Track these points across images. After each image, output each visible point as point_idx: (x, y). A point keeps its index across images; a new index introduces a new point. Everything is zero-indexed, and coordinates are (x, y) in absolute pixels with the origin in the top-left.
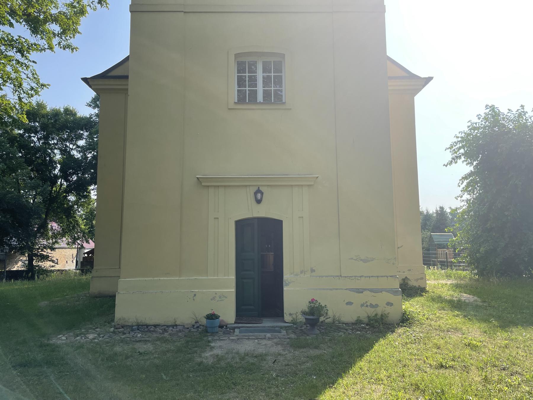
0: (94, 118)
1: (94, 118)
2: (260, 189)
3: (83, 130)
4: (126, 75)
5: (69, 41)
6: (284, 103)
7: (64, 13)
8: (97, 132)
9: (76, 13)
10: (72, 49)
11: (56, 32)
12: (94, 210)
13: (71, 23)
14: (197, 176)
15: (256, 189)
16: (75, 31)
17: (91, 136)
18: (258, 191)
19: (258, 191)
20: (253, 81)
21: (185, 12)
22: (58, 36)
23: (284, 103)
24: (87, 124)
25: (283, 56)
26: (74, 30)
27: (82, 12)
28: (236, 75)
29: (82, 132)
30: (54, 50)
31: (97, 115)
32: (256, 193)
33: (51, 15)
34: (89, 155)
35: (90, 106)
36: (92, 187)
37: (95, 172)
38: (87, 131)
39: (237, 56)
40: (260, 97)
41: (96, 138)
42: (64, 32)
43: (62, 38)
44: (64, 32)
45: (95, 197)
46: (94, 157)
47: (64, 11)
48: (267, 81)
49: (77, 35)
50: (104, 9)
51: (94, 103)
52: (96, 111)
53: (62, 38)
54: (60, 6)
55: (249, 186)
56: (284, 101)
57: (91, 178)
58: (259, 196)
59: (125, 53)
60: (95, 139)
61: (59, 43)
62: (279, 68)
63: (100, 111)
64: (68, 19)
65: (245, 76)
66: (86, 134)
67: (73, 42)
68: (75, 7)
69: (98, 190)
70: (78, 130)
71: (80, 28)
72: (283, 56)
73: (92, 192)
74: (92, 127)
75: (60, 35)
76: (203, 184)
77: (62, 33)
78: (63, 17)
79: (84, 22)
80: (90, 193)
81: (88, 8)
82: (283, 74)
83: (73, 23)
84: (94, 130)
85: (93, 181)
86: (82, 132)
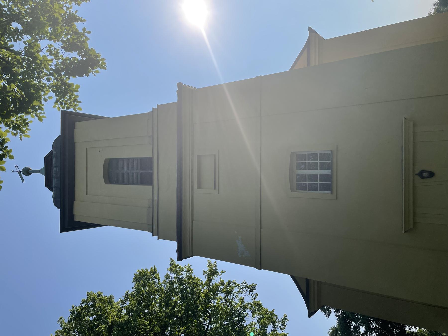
0: (339, 314)
1: (339, 314)
2: (417, 172)
3: (351, 326)
4: (305, 281)
5: (279, 321)
6: (331, 151)
7: (259, 319)
8: (353, 315)
9: (260, 311)
10: (286, 319)
11: (273, 329)
12: (431, 332)
13: (266, 316)
14: (403, 232)
15: (417, 177)
16: (272, 313)
17: (357, 320)
18: (421, 174)
19: (421, 174)
20: (314, 177)
21: (261, 228)
22: (276, 328)
23: (331, 151)
24: (344, 321)
25: (292, 153)
26: (271, 314)
27: (258, 305)
28: (307, 191)
29: (352, 327)
30: (286, 333)
31: (336, 311)
32: (423, 177)
33: (261, 330)
34: (374, 325)
35: (328, 315)
36: (407, 329)
37: (391, 323)
38: (352, 322)
39: (292, 190)
40: (327, 172)
41: (358, 316)
42: (273, 323)
43: (277, 326)
44: (273, 323)
45: (418, 328)
46: (376, 321)
47: (257, 319)
48: (311, 167)
49: (275, 313)
50: (257, 288)
51: (327, 311)
52: (333, 310)
53: (277, 326)
54: (254, 321)
55: (414, 183)
56: (330, 152)
57: (398, 329)
58: (425, 174)
59: (287, 278)
60: (359, 317)
61: (281, 329)
62: (302, 157)
63: (333, 307)
64: (263, 317)
65: (308, 184)
66: (353, 323)
67: (280, 317)
68: (255, 310)
69: (410, 324)
70: (350, 330)
71: (270, 310)
72: (292, 153)
73: (412, 330)
74: (347, 317)
75: (275, 327)
76: (412, 227)
77: (274, 325)
78: (262, 320)
79: (267, 305)
80: (413, 332)
81: (256, 300)
82: (318, 153)
83: (266, 314)
84: (350, 316)
85: (401, 327)
86: (352, 327)
